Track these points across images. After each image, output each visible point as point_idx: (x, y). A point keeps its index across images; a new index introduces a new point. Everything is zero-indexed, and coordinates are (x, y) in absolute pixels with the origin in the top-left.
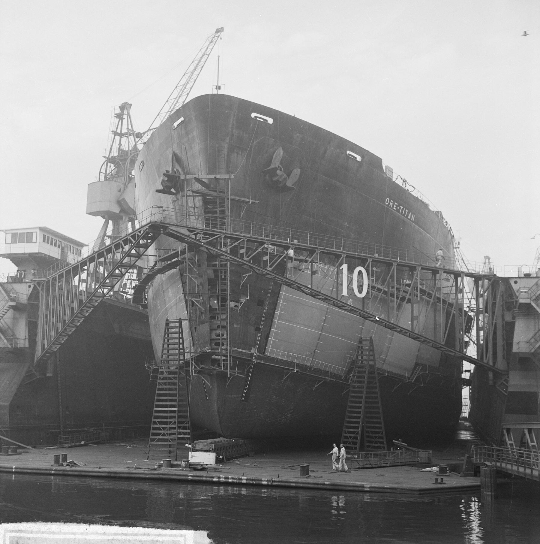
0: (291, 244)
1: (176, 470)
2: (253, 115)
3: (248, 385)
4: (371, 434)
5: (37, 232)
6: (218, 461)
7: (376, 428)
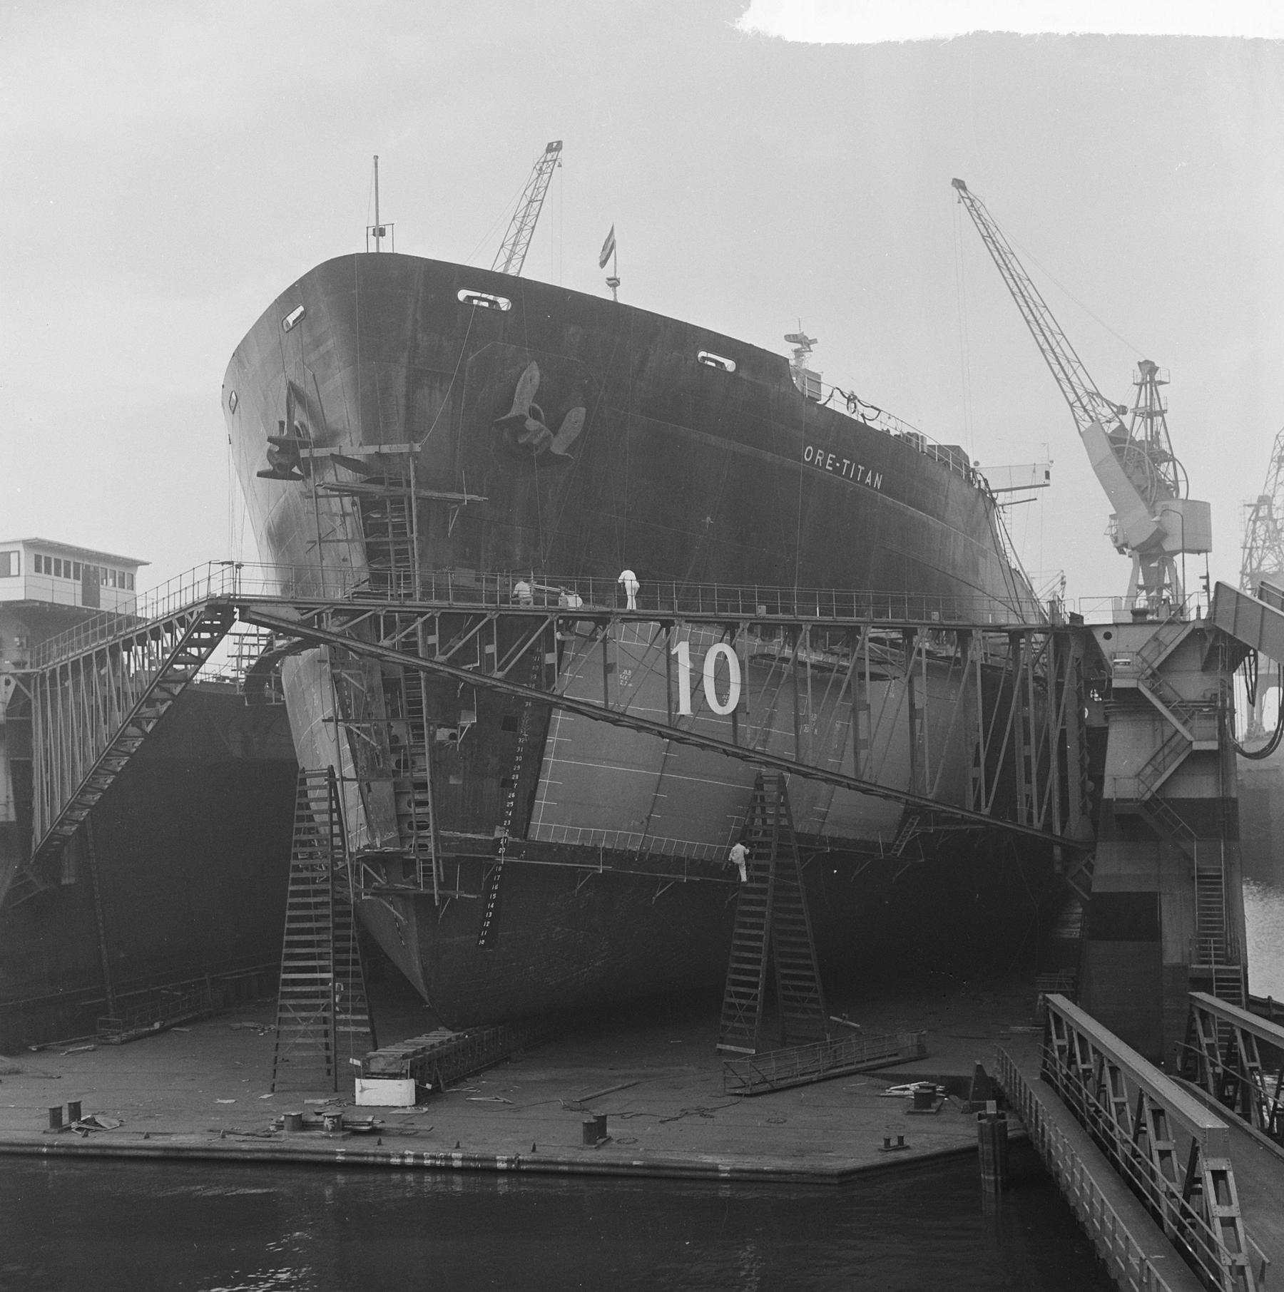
0: (549, 612)
1: (312, 1138)
2: (462, 295)
3: (491, 910)
4: (792, 993)
5: (19, 552)
6: (422, 1097)
7: (801, 978)
